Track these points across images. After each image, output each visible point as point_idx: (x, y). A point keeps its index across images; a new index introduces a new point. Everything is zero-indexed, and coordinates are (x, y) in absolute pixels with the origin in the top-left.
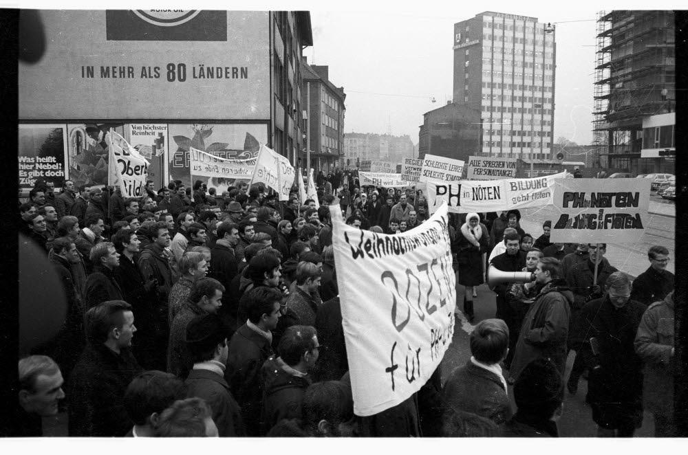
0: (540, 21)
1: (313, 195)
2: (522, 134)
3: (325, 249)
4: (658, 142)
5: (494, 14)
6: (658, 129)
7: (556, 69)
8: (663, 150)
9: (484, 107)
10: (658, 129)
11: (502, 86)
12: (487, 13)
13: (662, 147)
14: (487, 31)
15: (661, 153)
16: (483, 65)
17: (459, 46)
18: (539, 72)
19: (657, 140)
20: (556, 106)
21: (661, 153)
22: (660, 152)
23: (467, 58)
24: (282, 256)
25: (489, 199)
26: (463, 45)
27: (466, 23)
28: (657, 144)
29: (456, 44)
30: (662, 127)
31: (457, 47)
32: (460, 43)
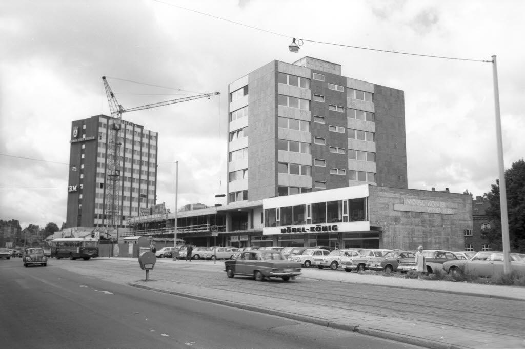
0: (145, 128)
1: (351, 259)
4: (310, 218)
7: (158, 167)
8: (285, 227)
10: (278, 209)
12: (103, 116)
13: (283, 225)
15: (283, 231)
17: (76, 141)
19: (278, 219)
20: (157, 198)
21: (283, 231)
22: (282, 229)
23: (82, 151)
24: (182, 241)
25: (287, 164)
26: (80, 140)
27: (82, 122)
29: (73, 138)
31: (74, 141)
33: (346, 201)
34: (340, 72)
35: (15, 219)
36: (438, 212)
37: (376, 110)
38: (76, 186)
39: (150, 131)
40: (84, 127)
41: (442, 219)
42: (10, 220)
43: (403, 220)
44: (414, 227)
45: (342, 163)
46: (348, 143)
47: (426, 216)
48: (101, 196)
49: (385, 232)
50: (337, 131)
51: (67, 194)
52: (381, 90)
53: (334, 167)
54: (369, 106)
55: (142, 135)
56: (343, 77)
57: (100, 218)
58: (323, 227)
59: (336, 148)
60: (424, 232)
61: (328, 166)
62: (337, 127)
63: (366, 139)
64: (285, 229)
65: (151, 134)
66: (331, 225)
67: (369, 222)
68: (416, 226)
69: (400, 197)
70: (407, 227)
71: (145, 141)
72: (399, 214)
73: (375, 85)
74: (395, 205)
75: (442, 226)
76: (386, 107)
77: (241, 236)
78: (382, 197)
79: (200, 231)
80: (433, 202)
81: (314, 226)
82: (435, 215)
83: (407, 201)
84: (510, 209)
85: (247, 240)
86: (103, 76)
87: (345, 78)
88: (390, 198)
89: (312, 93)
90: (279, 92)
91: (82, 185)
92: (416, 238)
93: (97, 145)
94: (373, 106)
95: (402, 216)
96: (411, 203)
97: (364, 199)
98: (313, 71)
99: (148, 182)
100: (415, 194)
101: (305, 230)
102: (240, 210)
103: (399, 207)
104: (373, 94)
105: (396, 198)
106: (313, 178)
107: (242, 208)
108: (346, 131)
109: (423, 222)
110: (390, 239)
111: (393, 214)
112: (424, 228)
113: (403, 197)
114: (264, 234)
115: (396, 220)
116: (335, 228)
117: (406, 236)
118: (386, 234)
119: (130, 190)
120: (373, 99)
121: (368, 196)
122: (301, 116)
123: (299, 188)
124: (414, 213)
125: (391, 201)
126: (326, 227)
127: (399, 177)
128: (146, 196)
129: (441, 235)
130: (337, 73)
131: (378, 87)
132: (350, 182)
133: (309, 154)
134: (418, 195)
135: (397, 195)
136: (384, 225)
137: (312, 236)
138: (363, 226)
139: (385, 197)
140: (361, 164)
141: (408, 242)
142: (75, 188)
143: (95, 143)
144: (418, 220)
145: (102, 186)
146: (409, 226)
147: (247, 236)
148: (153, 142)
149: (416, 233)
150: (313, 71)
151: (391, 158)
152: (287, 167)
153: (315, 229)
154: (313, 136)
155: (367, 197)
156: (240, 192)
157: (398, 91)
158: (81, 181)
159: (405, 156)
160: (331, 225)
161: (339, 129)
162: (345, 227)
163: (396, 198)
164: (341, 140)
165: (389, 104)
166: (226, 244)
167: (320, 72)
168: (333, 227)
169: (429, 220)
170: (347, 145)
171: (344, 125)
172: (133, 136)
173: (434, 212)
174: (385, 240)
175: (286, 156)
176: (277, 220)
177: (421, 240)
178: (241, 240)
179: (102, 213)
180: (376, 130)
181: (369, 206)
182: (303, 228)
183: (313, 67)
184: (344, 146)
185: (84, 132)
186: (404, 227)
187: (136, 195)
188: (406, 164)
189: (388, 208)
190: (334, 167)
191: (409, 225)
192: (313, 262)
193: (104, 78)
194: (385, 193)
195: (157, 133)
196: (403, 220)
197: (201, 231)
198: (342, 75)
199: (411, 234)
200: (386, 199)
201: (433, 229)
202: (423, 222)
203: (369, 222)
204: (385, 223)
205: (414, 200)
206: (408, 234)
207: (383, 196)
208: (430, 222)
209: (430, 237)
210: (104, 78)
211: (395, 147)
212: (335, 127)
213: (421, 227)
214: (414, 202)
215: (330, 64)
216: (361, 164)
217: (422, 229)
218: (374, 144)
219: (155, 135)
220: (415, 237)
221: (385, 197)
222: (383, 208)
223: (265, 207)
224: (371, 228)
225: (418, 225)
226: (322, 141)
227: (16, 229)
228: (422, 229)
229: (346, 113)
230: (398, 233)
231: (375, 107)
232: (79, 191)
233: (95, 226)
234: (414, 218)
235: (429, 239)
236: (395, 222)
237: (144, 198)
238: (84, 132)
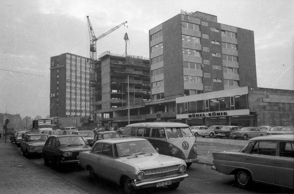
2: (76, 111)
3: (185, 95)
5: (71, 55)
6: (186, 103)
9: (67, 110)
11: (76, 83)
12: (68, 53)
14: (68, 61)
16: (66, 101)
18: (78, 103)
21: (190, 116)
22: (189, 115)
28: (186, 111)
29: (51, 66)
30: (197, 101)
31: (52, 68)
32: (54, 66)
33: (233, 97)
35: (18, 113)
36: (287, 103)
37: (238, 43)
38: (55, 94)
40: (58, 60)
41: (290, 106)
42: (13, 114)
43: (268, 108)
44: (274, 112)
45: (219, 74)
47: (281, 105)
49: (258, 115)
51: (49, 98)
54: (234, 41)
57: (79, 112)
58: (217, 113)
60: (280, 115)
62: (216, 54)
63: (196, 68)
64: (191, 115)
68: (275, 111)
70: (270, 112)
72: (266, 104)
75: (290, 111)
81: (211, 113)
82: (286, 104)
83: (270, 96)
84: (240, 108)
87: (220, 24)
91: (58, 93)
101: (205, 115)
102: (160, 105)
106: (203, 85)
108: (222, 56)
109: (279, 108)
111: (262, 104)
112: (280, 112)
115: (264, 107)
118: (259, 116)
121: (248, 93)
123: (196, 90)
125: (261, 96)
126: (219, 113)
130: (216, 22)
131: (239, 29)
132: (225, 86)
134: (276, 92)
138: (245, 112)
140: (230, 75)
142: (54, 95)
144: (276, 108)
153: (212, 115)
155: (247, 94)
156: (155, 95)
157: (250, 31)
158: (58, 91)
160: (223, 112)
161: (217, 55)
162: (231, 113)
164: (218, 61)
165: (245, 39)
168: (224, 113)
176: (231, 106)
179: (75, 109)
182: (204, 114)
185: (58, 63)
192: (199, 133)
193: (88, 17)
196: (268, 108)
198: (218, 22)
201: (285, 112)
202: (279, 108)
204: (258, 110)
205: (274, 96)
208: (283, 109)
210: (88, 17)
216: (230, 75)
220: (275, 118)
223: (177, 102)
224: (251, 113)
225: (277, 111)
227: (18, 119)
229: (221, 45)
232: (57, 97)
235: (283, 119)
238: (58, 63)
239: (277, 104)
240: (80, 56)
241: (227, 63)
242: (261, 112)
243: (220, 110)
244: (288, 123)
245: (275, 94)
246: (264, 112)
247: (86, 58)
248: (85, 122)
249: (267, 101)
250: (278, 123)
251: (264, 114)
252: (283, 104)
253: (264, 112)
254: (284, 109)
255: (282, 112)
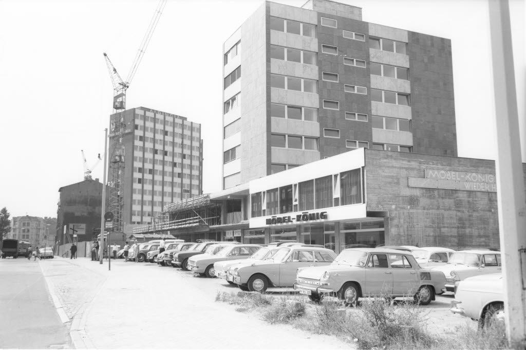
15: (268, 222)
21: (268, 222)
34: (361, 17)
36: (483, 190)
39: (192, 123)
46: (372, 108)
47: (463, 196)
48: (169, 194)
49: (392, 219)
50: (356, 92)
52: (418, 39)
53: (352, 138)
54: (402, 60)
55: (183, 126)
56: (364, 22)
59: (355, 114)
60: (460, 219)
61: (343, 137)
62: (356, 87)
65: (193, 125)
66: (320, 211)
67: (365, 205)
69: (418, 168)
70: (430, 211)
71: (187, 132)
72: (417, 193)
73: (408, 31)
74: (410, 179)
75: (490, 211)
76: (426, 60)
77: (234, 231)
78: (388, 167)
79: (183, 226)
80: (474, 174)
85: (240, 235)
86: (104, 52)
88: (403, 168)
89: (319, 42)
90: (272, 42)
92: (446, 229)
93: (134, 138)
94: (408, 60)
95: (423, 195)
96: (434, 173)
97: (356, 171)
98: (320, 15)
99: (191, 177)
100: (444, 163)
102: (229, 197)
103: (413, 182)
104: (407, 43)
105: (412, 169)
107: (231, 195)
109: (458, 204)
110: (402, 230)
111: (407, 192)
112: (459, 214)
113: (423, 167)
114: (250, 227)
115: (413, 201)
116: (323, 216)
117: (428, 225)
118: (395, 222)
119: (152, 184)
120: (407, 50)
121: (364, 165)
122: (303, 73)
124: (444, 191)
125: (404, 173)
126: (314, 214)
127: (446, 151)
128: (189, 191)
129: (488, 224)
130: (357, 18)
131: (413, 35)
133: (317, 122)
135: (413, 163)
136: (391, 208)
137: (297, 229)
138: (356, 212)
139: (393, 167)
141: (432, 234)
143: (130, 136)
144: (448, 202)
145: (140, 181)
146: (434, 211)
147: (240, 230)
148: (195, 134)
149: (446, 221)
150: (320, 15)
151: (433, 126)
152: (302, 141)
154: (320, 99)
155: (363, 167)
157: (442, 39)
159: (454, 124)
162: (337, 214)
163: (412, 169)
166: (222, 239)
167: (330, 16)
168: (322, 214)
169: (469, 202)
170: (371, 110)
171: (367, 83)
172: (183, 129)
173: (475, 189)
174: (393, 231)
175: (283, 125)
177: (454, 232)
178: (235, 236)
180: (412, 89)
181: (367, 179)
182: (289, 217)
183: (322, 10)
184: (365, 110)
186: (425, 211)
187: (177, 190)
188: (455, 135)
189: (398, 183)
190: (352, 138)
191: (433, 209)
194: (394, 161)
195: (200, 125)
196: (424, 201)
197: (185, 226)
199: (438, 223)
200: (394, 169)
201: (475, 214)
202: (458, 204)
203: (365, 205)
204: (394, 207)
205: (443, 172)
206: (433, 222)
207: (391, 165)
209: (469, 227)
211: (439, 113)
212: (354, 87)
213: (455, 212)
214: (443, 175)
215: (341, 5)
217: (456, 215)
218: (409, 109)
219: (198, 126)
220: (444, 227)
221: (393, 167)
222: (390, 183)
224: (369, 214)
225: (450, 209)
226: (335, 105)
228: (456, 215)
230: (415, 221)
231: (410, 60)
233: (134, 223)
234: (443, 198)
235: (468, 231)
236: (410, 204)
237: (186, 194)
239: (451, 193)
240: (162, 112)
241: (379, 108)
242: (401, 211)
243: (318, 207)
244: (483, 239)
245: (448, 168)
246: (411, 211)
247: (174, 115)
248: (79, 233)
249: (422, 186)
250: (454, 239)
251: (410, 216)
252: (470, 193)
253: (411, 211)
254: (472, 207)
255: (466, 215)
